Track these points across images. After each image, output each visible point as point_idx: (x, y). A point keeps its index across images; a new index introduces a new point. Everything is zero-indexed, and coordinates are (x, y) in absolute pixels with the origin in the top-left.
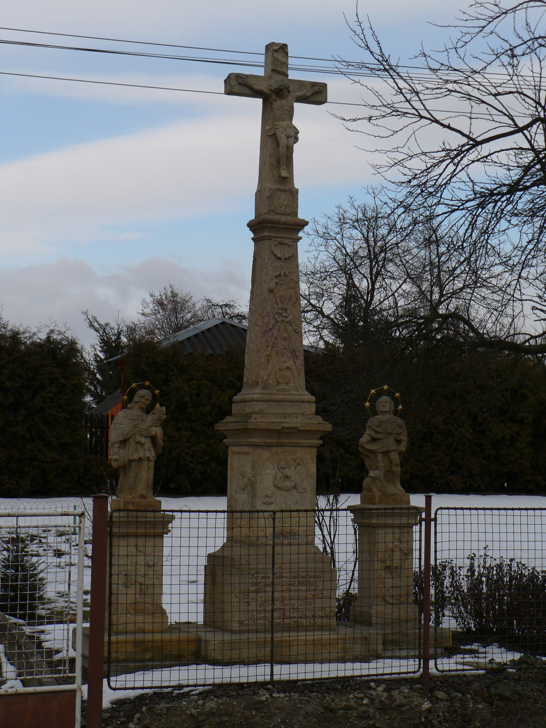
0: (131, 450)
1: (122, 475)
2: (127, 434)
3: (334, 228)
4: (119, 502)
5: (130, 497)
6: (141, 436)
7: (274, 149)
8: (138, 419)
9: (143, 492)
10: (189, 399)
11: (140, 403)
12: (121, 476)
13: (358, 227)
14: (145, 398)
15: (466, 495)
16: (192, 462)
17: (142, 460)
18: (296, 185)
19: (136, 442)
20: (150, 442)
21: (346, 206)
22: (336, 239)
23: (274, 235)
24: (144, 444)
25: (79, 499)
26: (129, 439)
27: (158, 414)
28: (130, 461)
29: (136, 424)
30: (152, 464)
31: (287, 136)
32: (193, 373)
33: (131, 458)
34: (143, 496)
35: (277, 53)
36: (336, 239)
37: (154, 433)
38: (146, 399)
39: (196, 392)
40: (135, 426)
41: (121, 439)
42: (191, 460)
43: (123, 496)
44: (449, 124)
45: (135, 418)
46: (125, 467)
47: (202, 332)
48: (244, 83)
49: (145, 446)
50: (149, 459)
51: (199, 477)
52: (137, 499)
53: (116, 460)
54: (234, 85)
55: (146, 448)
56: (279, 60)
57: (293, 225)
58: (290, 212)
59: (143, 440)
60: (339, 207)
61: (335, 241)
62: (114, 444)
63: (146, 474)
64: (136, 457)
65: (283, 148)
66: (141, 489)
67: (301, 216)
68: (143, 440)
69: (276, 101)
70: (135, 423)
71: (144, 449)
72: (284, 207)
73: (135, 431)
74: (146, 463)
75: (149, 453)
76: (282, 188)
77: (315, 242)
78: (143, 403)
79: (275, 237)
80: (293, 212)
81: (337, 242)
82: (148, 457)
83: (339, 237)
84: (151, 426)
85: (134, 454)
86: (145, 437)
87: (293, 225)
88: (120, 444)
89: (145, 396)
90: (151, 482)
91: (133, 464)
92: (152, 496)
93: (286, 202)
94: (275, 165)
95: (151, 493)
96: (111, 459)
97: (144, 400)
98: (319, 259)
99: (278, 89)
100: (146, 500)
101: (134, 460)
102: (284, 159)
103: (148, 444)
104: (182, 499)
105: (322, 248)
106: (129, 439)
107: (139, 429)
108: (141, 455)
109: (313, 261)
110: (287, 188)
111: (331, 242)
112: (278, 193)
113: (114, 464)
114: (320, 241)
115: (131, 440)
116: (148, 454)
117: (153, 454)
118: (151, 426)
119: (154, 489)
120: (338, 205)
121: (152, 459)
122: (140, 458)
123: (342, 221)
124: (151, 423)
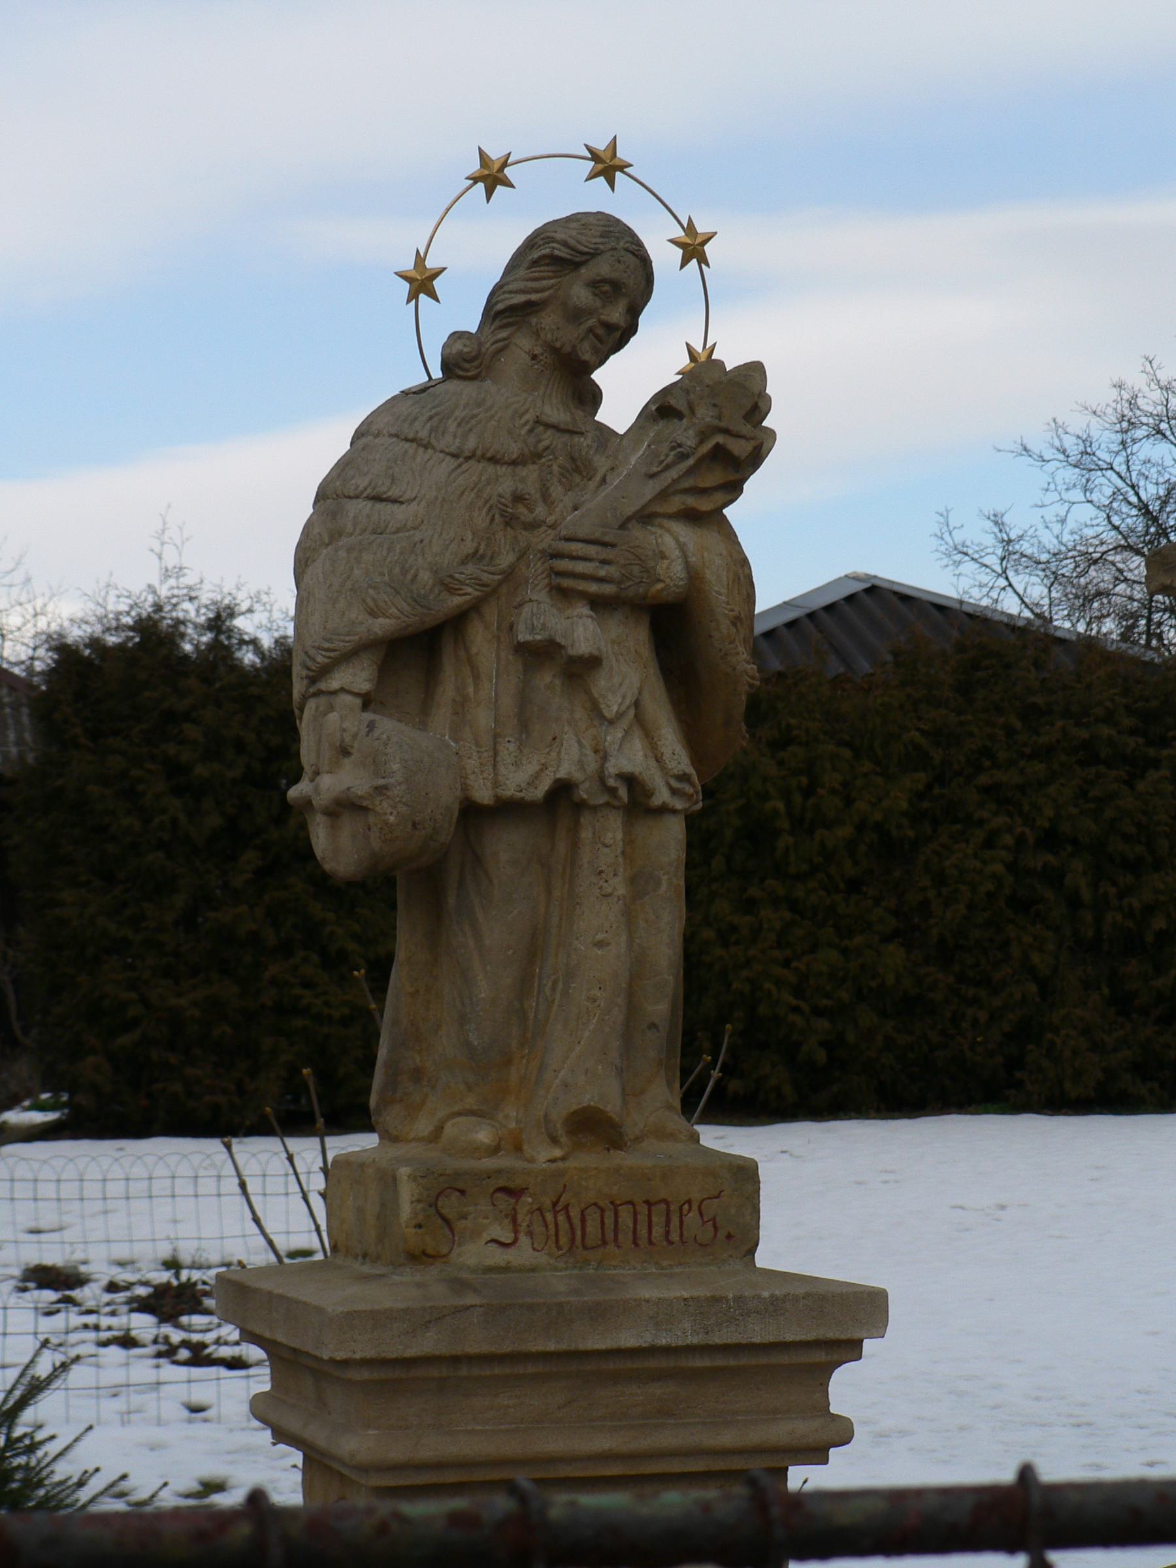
0: (483, 718)
1: (407, 946)
2: (448, 586)
3: (1106, 440)
4: (388, 1181)
5: (484, 1136)
6: (563, 595)
8: (536, 456)
9: (600, 1091)
10: (781, 806)
11: (548, 320)
12: (401, 954)
13: (1168, 433)
14: (587, 273)
15: (741, 1124)
16: (796, 1009)
17: (580, 806)
19: (522, 649)
20: (646, 651)
21: (1137, 380)
22: (1112, 468)
24: (593, 662)
25: (213, 1146)
26: (457, 622)
27: (705, 415)
28: (472, 815)
29: (518, 498)
30: (669, 840)
32: (793, 721)
33: (483, 795)
34: (591, 1127)
36: (1112, 468)
37: (672, 573)
38: (594, 285)
39: (804, 780)
40: (511, 515)
41: (381, 626)
42: (795, 1002)
43: (423, 1126)
45: (514, 449)
46: (435, 869)
47: (811, 616)
49: (601, 683)
50: (636, 801)
51: (821, 1056)
52: (543, 1154)
53: (346, 807)
55: (612, 707)
59: (582, 632)
60: (1120, 386)
61: (1109, 473)
62: (325, 671)
63: (620, 925)
64: (522, 777)
66: (578, 1064)
68: (582, 632)
70: (506, 483)
71: (595, 709)
73: (506, 560)
74: (613, 829)
75: (637, 746)
77: (1059, 480)
78: (576, 315)
81: (1114, 477)
82: (630, 780)
83: (1119, 463)
84: (645, 517)
85: (508, 749)
86: (599, 604)
88: (385, 671)
89: (594, 254)
90: (660, 1007)
91: (505, 847)
92: (676, 1122)
95: (662, 1094)
96: (308, 804)
97: (581, 295)
98: (1071, 524)
100: (618, 1158)
101: (509, 809)
103: (628, 671)
104: (890, 1122)
105: (1077, 495)
106: (457, 622)
107: (543, 540)
108: (569, 760)
109: (1057, 528)
111: (1098, 478)
113: (336, 849)
114: (1071, 474)
115: (481, 639)
116: (631, 757)
117: (678, 757)
118: (645, 517)
119: (685, 1072)
120: (1115, 380)
121: (663, 796)
122: (562, 790)
123: (1127, 424)
124: (651, 489)
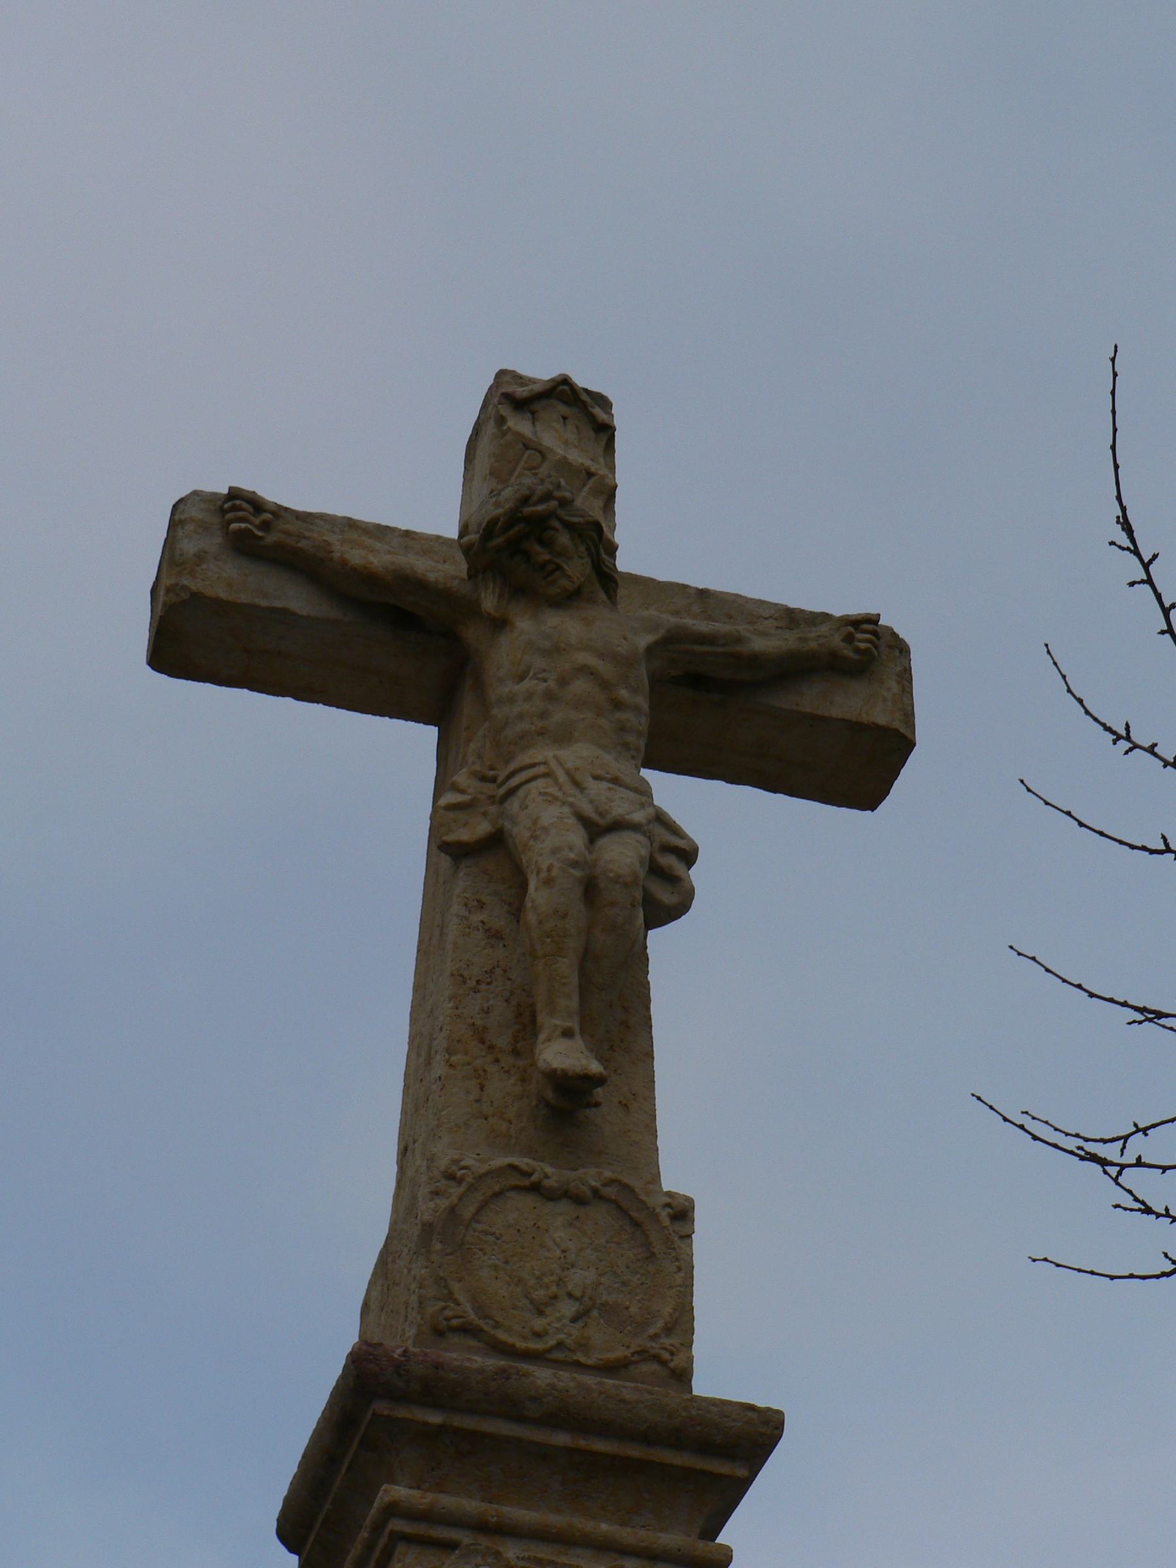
7: (494, 936)
18: (675, 1175)
23: (471, 1505)
31: (584, 821)
35: (546, 448)
44: (1146, 1135)
48: (270, 538)
54: (200, 557)
56: (542, 453)
57: (648, 1438)
58: (619, 1353)
65: (549, 882)
67: (723, 1369)
69: (500, 624)
72: (568, 1309)
76: (551, 1173)
79: (482, 1527)
80: (644, 1355)
87: (648, 1438)
93: (579, 1278)
94: (503, 1042)
99: (514, 517)
102: (567, 967)
110: (590, 1176)
112: (519, 1209)
